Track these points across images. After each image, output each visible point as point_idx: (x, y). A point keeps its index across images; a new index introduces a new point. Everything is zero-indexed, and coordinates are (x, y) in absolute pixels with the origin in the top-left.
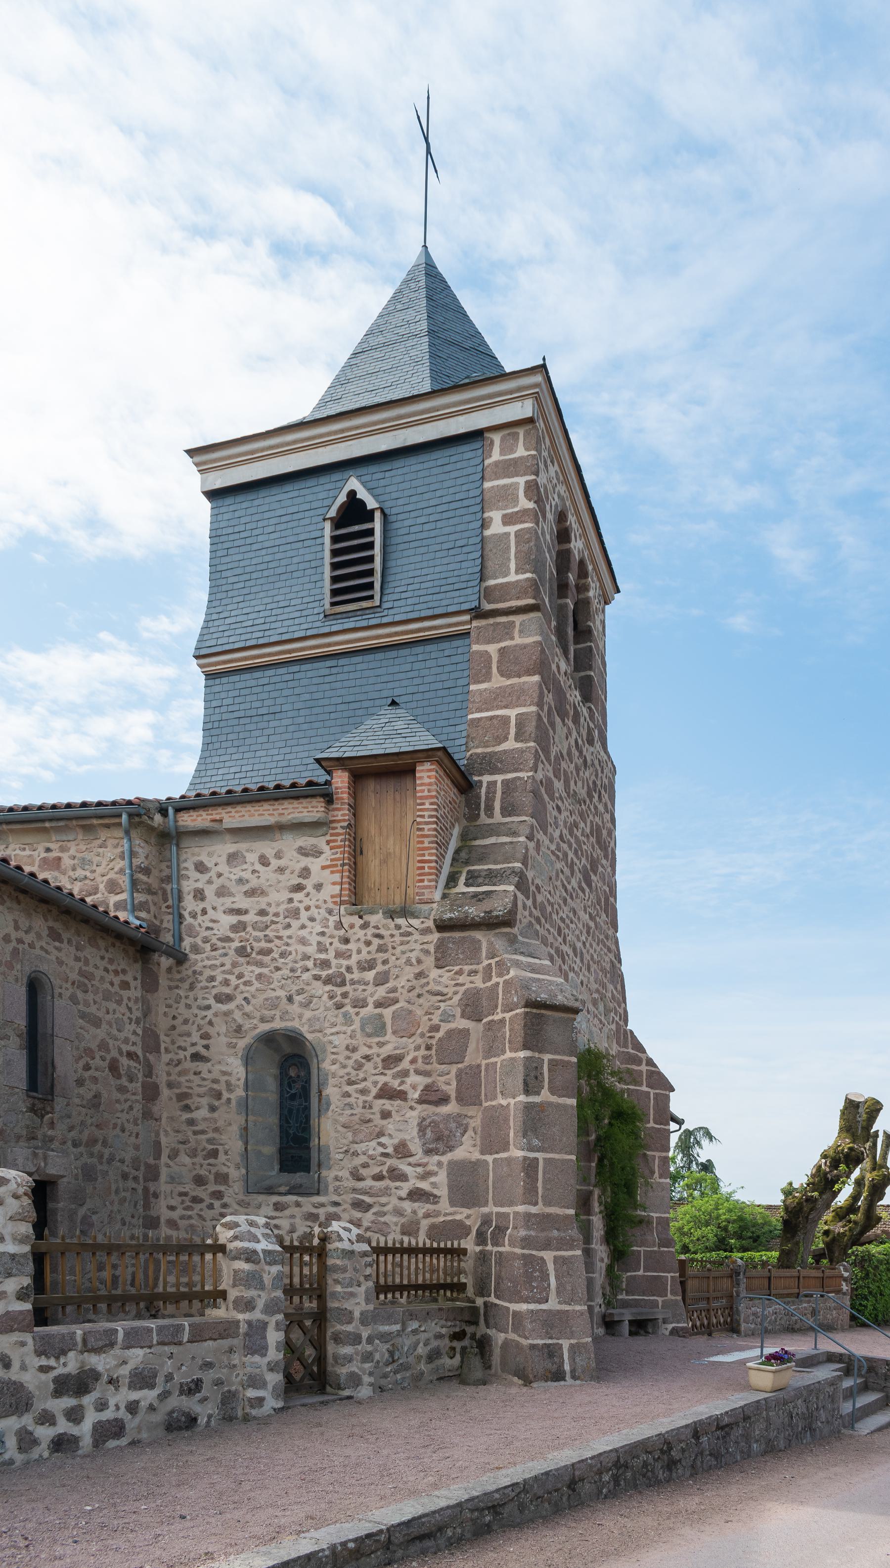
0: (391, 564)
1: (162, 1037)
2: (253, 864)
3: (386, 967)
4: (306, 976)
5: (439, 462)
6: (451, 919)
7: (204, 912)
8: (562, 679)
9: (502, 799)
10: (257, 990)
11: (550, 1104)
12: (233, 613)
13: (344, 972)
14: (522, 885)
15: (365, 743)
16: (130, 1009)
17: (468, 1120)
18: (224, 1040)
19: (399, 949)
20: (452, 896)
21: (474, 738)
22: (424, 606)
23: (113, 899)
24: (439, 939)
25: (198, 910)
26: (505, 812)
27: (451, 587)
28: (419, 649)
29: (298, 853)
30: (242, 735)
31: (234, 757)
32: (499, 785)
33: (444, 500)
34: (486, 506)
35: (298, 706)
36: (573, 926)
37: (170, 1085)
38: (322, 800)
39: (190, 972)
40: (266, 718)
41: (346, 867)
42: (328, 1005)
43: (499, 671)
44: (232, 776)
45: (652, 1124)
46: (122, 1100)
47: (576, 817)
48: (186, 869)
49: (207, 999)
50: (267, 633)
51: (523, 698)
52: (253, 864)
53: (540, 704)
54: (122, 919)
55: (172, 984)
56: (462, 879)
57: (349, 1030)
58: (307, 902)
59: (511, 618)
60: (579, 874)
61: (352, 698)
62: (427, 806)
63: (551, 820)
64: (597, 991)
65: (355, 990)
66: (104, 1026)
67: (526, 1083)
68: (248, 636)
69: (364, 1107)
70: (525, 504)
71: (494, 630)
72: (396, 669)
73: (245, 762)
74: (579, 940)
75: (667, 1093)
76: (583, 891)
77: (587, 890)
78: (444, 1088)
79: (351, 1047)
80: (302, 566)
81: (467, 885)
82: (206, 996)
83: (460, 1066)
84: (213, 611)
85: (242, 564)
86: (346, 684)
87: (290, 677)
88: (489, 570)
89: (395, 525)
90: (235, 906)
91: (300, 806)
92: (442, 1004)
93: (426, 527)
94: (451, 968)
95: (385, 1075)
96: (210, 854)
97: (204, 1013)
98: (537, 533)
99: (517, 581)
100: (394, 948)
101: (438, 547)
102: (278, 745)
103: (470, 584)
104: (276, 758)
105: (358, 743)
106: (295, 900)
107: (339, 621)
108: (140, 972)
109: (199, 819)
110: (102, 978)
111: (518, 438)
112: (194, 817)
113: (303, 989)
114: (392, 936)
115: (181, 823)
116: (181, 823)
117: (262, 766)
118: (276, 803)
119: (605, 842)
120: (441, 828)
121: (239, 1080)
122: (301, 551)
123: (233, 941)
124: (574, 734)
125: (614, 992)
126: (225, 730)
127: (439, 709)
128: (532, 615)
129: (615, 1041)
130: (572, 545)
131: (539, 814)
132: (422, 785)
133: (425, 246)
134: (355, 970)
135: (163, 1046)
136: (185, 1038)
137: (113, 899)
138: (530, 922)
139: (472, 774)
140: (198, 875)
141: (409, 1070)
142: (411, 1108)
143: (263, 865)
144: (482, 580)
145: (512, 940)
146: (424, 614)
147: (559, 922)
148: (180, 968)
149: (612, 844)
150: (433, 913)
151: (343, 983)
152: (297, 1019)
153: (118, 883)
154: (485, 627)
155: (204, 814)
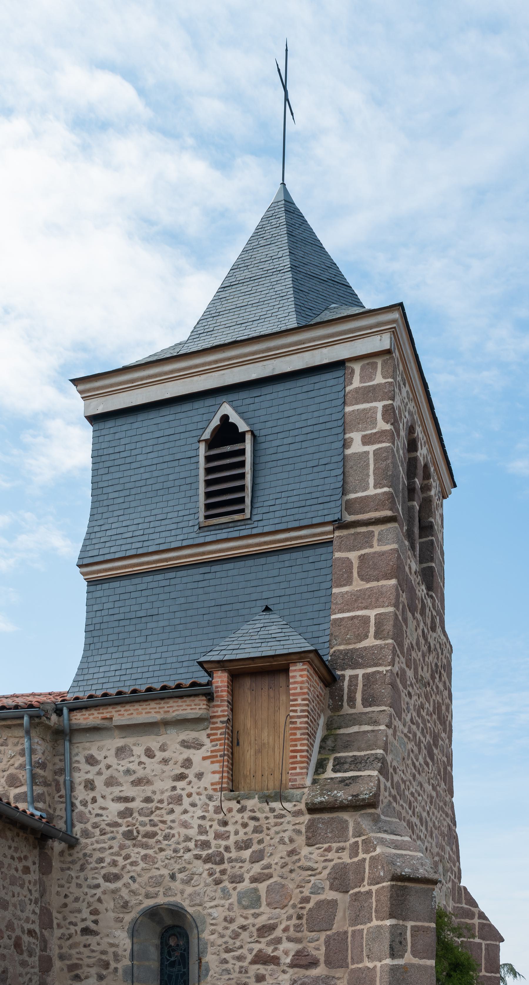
0: (259, 480)
1: (55, 914)
2: (139, 756)
3: (261, 846)
4: (188, 856)
5: (305, 389)
6: (322, 802)
7: (94, 800)
8: (412, 578)
9: (363, 691)
10: (143, 869)
11: (412, 965)
12: (114, 526)
13: (223, 851)
14: (383, 771)
15: (243, 646)
16: (30, 891)
17: (336, 981)
18: (111, 915)
19: (273, 830)
20: (321, 782)
21: (337, 636)
22: (292, 518)
23: (13, 792)
24: (309, 820)
25: (89, 799)
26: (367, 702)
27: (315, 501)
28: (286, 557)
29: (181, 746)
30: (121, 636)
31: (114, 656)
32: (360, 678)
33: (309, 422)
34: (347, 428)
35: (173, 609)
36: (420, 798)
37: (62, 957)
38: (204, 698)
39: (81, 855)
40: (144, 620)
41: (226, 758)
42: (207, 882)
43: (359, 576)
44: (113, 674)
45: (483, 973)
46: (24, 973)
47: (422, 700)
48: (78, 762)
49: (97, 878)
50: (146, 544)
51: (381, 600)
52: (139, 756)
53: (396, 606)
54: (21, 809)
55: (64, 866)
56: (330, 766)
57: (227, 903)
58: (189, 789)
59: (371, 528)
60: (424, 750)
61: (223, 601)
62: (299, 702)
63: (404, 706)
64: (438, 854)
65: (233, 867)
66: (11, 908)
67: (392, 948)
68: (128, 547)
69: (240, 972)
70: (382, 425)
71: (355, 539)
72: (265, 574)
73: (125, 660)
74: (424, 810)
75: (497, 943)
76: (427, 765)
77: (431, 763)
78: (314, 952)
79: (228, 919)
80: (177, 483)
81: (334, 770)
82: (96, 876)
83: (328, 933)
84: (94, 523)
85: (122, 481)
86: (218, 588)
87: (167, 583)
88: (349, 487)
89: (263, 446)
90: (123, 795)
91: (184, 704)
92: (312, 878)
93: (292, 447)
94: (321, 845)
95: (260, 942)
96: (100, 749)
97: (94, 891)
98: (393, 451)
99: (375, 495)
100: (268, 829)
101: (303, 465)
102: (155, 644)
103: (333, 498)
104: (153, 656)
105: (237, 647)
106: (178, 788)
107: (212, 532)
108: (38, 857)
109: (91, 717)
110: (9, 865)
111: (376, 368)
112: (87, 716)
113: (184, 868)
114: (267, 818)
115: (74, 721)
116: (74, 721)
117: (141, 664)
118: (162, 702)
119: (444, 718)
120: (311, 721)
121: (125, 950)
122: (177, 469)
123: (121, 826)
124: (422, 624)
125: (451, 853)
126: (106, 632)
127: (304, 609)
128: (390, 525)
129: (451, 898)
130: (418, 454)
131: (395, 704)
132: (295, 683)
133: (283, 184)
134: (233, 849)
135: (55, 922)
136: (76, 915)
137: (13, 792)
138: (390, 801)
139: (335, 669)
140: (88, 767)
141: (281, 938)
142: (284, 972)
143: (149, 757)
144: (344, 493)
145: (376, 820)
146: (290, 525)
147: (409, 796)
148: (71, 852)
149: (449, 718)
150: (305, 797)
151: (222, 862)
152: (179, 895)
153: (18, 778)
154: (347, 537)
155: (95, 713)
